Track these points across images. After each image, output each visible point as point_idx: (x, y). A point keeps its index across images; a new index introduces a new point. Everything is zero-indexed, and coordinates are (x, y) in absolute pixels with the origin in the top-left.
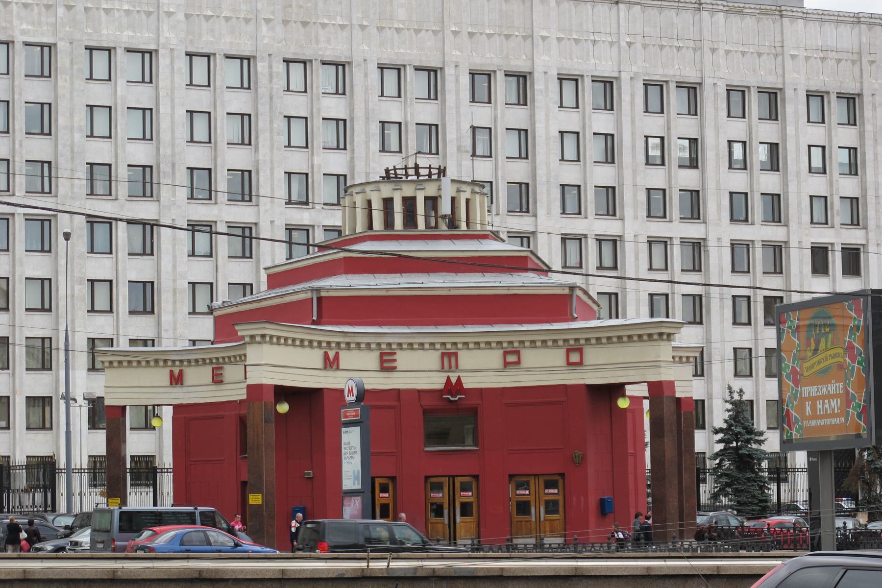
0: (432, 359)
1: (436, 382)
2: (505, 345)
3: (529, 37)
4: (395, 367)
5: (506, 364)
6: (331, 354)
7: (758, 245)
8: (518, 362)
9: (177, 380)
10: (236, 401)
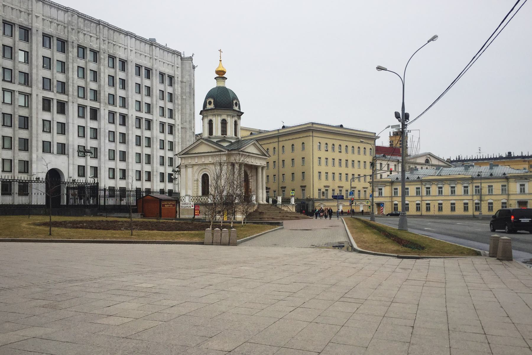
7: (167, 125)
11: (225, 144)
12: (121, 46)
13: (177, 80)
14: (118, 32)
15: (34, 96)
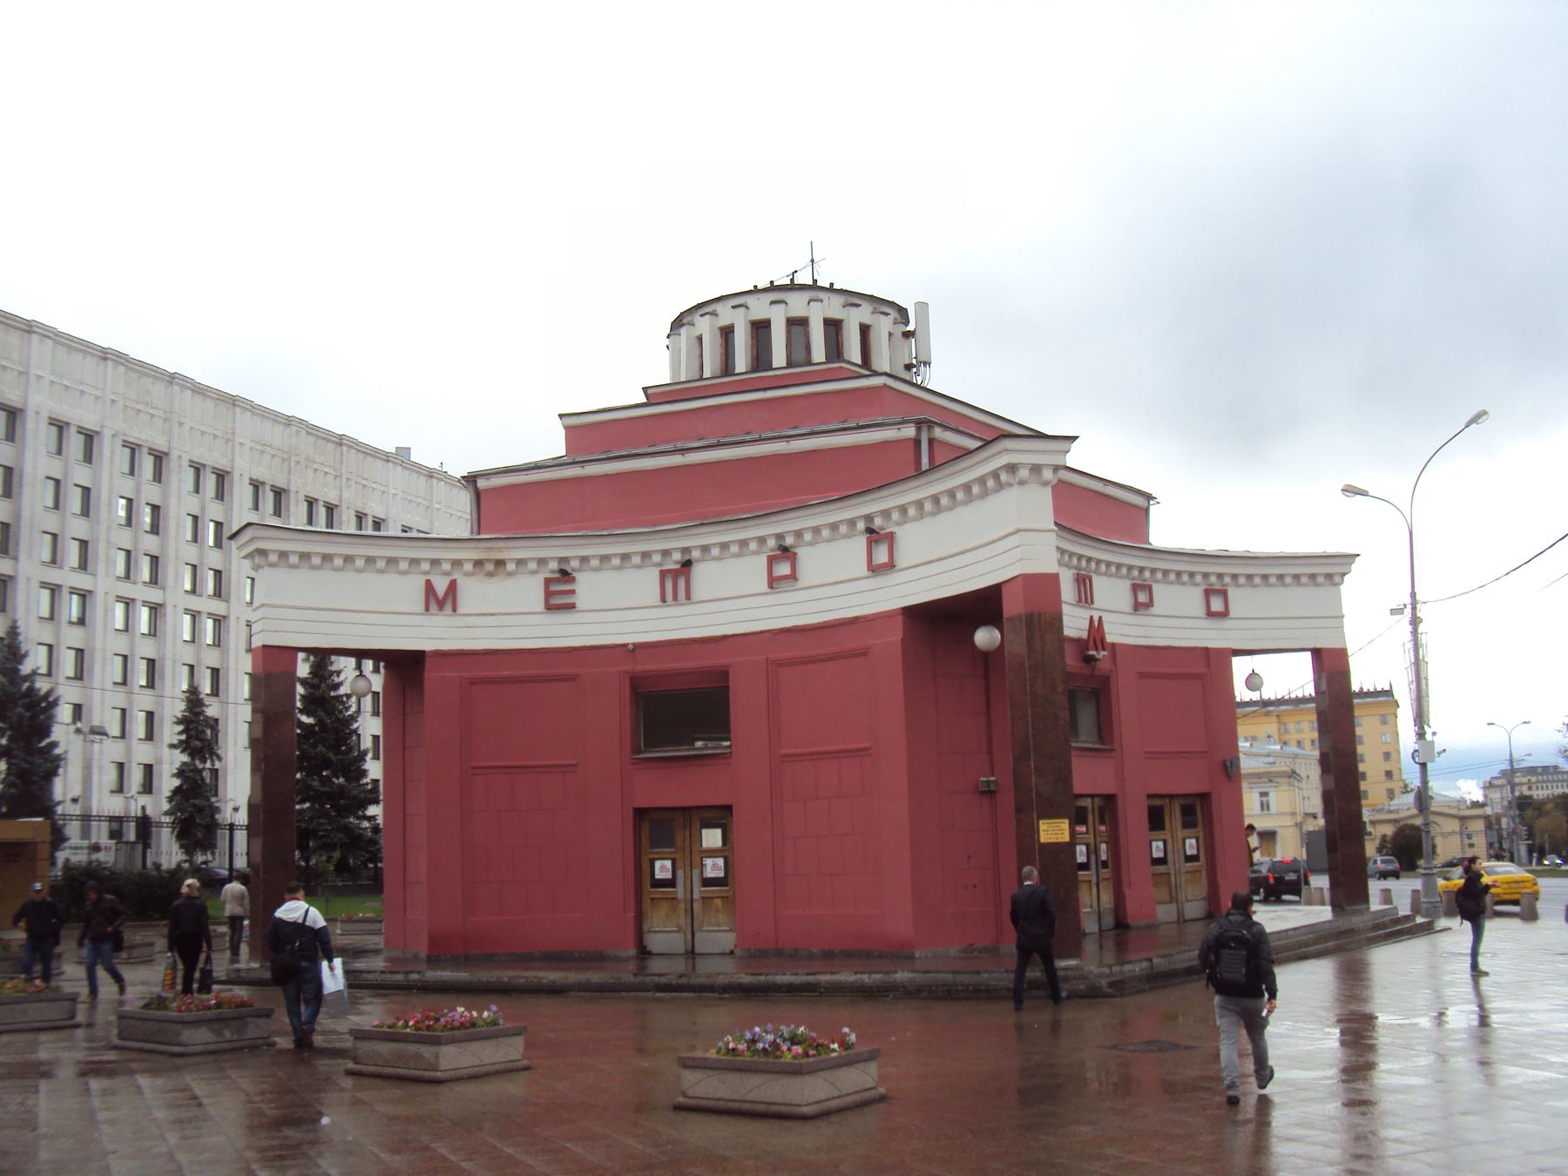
3: (25, 374)
9: (441, 600)
12: (155, 413)
14: (372, 456)
15: (232, 621)
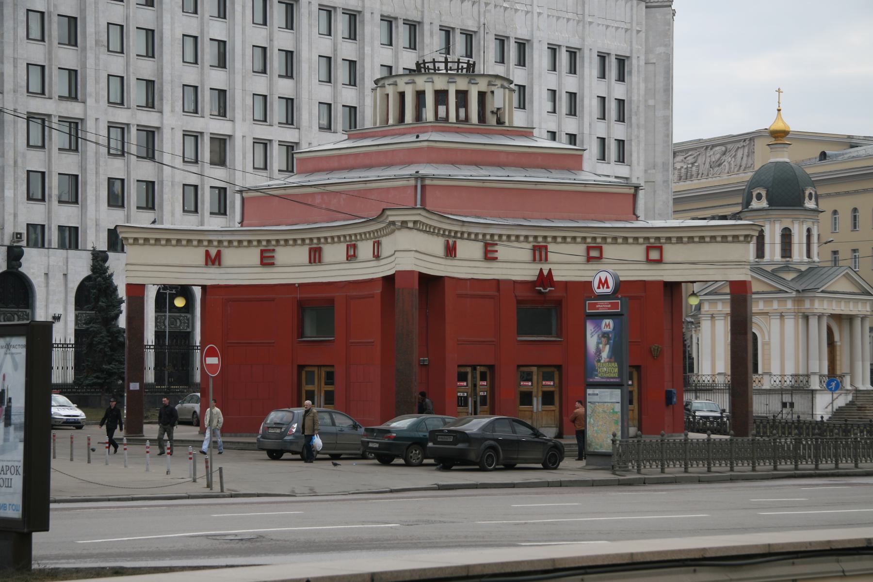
0: (523, 252)
1: (527, 272)
2: (589, 240)
4: (496, 258)
5: (589, 259)
6: (451, 242)
8: (601, 257)
9: (213, 260)
10: (295, 284)
11: (790, 276)
13: (636, 65)
